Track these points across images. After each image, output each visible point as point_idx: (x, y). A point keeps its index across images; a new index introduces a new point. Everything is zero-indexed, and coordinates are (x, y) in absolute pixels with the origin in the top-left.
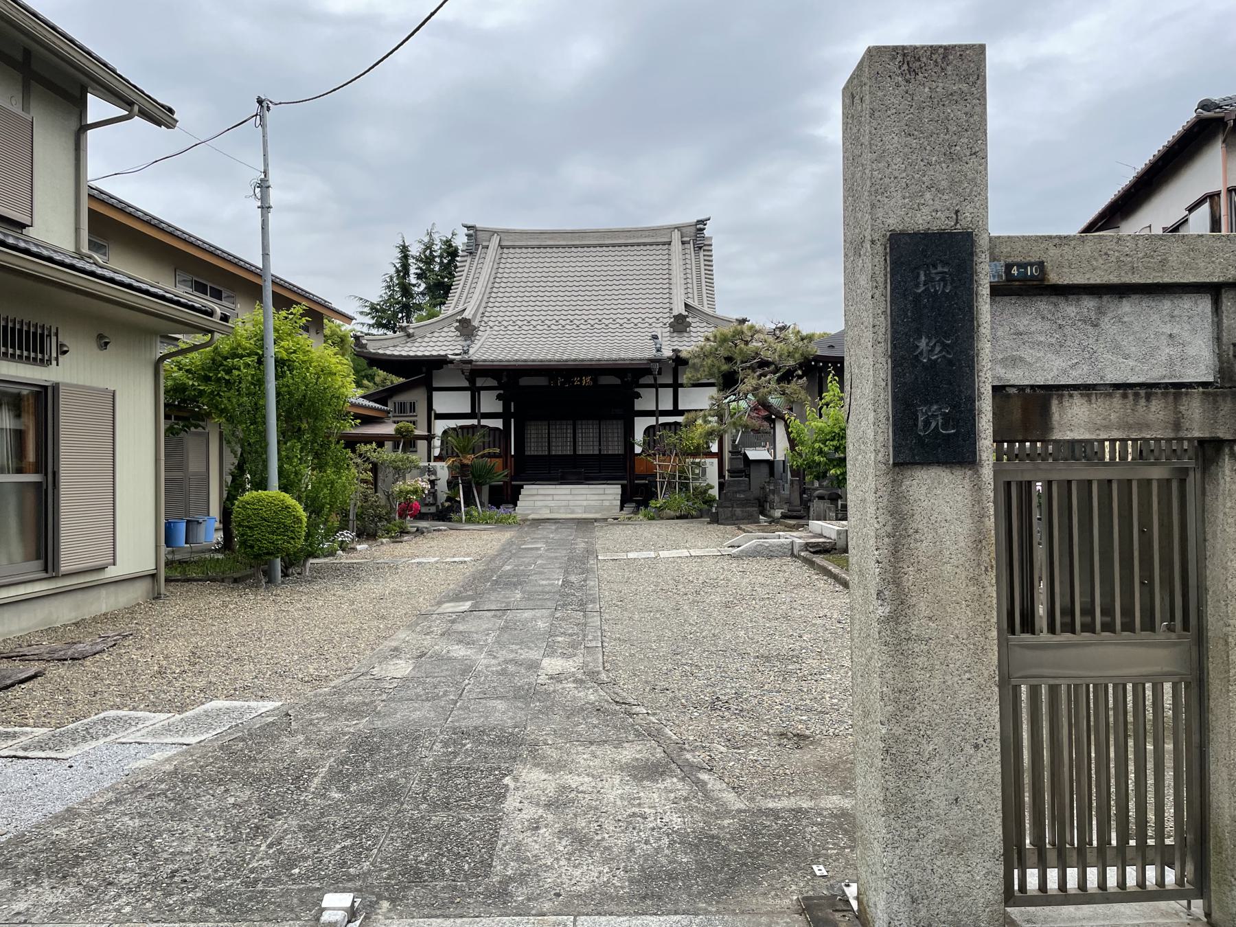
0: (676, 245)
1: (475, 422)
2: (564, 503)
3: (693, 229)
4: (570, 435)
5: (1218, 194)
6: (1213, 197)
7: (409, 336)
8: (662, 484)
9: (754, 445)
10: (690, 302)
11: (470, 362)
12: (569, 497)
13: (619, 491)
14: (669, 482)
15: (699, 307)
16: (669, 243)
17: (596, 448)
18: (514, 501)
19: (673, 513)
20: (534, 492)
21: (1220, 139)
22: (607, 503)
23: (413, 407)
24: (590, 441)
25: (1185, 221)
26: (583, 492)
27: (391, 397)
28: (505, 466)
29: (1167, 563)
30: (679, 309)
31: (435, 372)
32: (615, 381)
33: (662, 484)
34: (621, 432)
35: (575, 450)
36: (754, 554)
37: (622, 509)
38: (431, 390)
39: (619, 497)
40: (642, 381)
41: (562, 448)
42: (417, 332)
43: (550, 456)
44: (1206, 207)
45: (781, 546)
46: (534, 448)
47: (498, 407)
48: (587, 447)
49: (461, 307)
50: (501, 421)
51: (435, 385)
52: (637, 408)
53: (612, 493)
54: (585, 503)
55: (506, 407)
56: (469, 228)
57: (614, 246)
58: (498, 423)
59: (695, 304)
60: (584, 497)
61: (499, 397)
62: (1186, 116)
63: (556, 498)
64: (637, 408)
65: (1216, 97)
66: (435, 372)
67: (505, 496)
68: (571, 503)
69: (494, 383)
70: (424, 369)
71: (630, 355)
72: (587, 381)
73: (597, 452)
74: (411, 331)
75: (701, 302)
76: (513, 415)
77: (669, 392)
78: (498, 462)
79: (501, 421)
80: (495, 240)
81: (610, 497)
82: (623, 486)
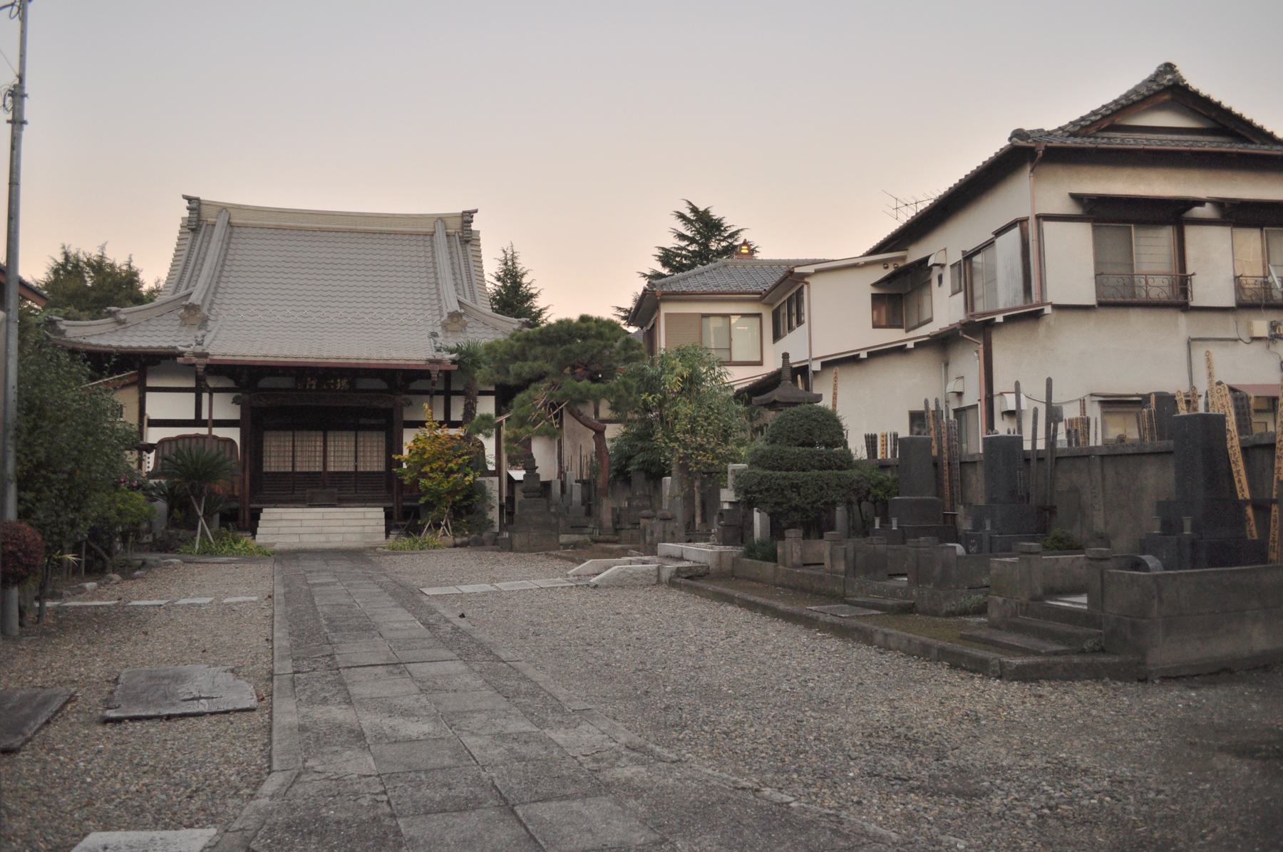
0: (441, 239)
1: (203, 431)
3: (459, 220)
5: (1026, 220)
6: (1020, 223)
7: (121, 322)
9: (156, 458)
10: (462, 299)
11: (206, 355)
12: (321, 523)
13: (382, 515)
15: (474, 305)
16: (432, 235)
18: (252, 525)
20: (277, 516)
21: (1029, 168)
24: (345, 453)
25: (990, 244)
30: (455, 307)
32: (379, 384)
34: (383, 445)
35: (293, 466)
36: (620, 584)
37: (387, 537)
38: (143, 390)
39: (383, 522)
40: (413, 386)
42: (129, 318)
43: (294, 473)
44: (1015, 233)
45: (646, 572)
47: (234, 413)
49: (182, 292)
51: (150, 384)
53: (373, 517)
56: (190, 199)
58: (234, 434)
59: (468, 301)
61: (235, 401)
62: (997, 143)
63: (305, 523)
65: (1028, 127)
67: (241, 519)
69: (231, 384)
70: (137, 365)
71: (405, 356)
72: (342, 384)
73: (352, 469)
74: (122, 317)
75: (474, 299)
77: (440, 400)
81: (373, 523)
82: (385, 509)
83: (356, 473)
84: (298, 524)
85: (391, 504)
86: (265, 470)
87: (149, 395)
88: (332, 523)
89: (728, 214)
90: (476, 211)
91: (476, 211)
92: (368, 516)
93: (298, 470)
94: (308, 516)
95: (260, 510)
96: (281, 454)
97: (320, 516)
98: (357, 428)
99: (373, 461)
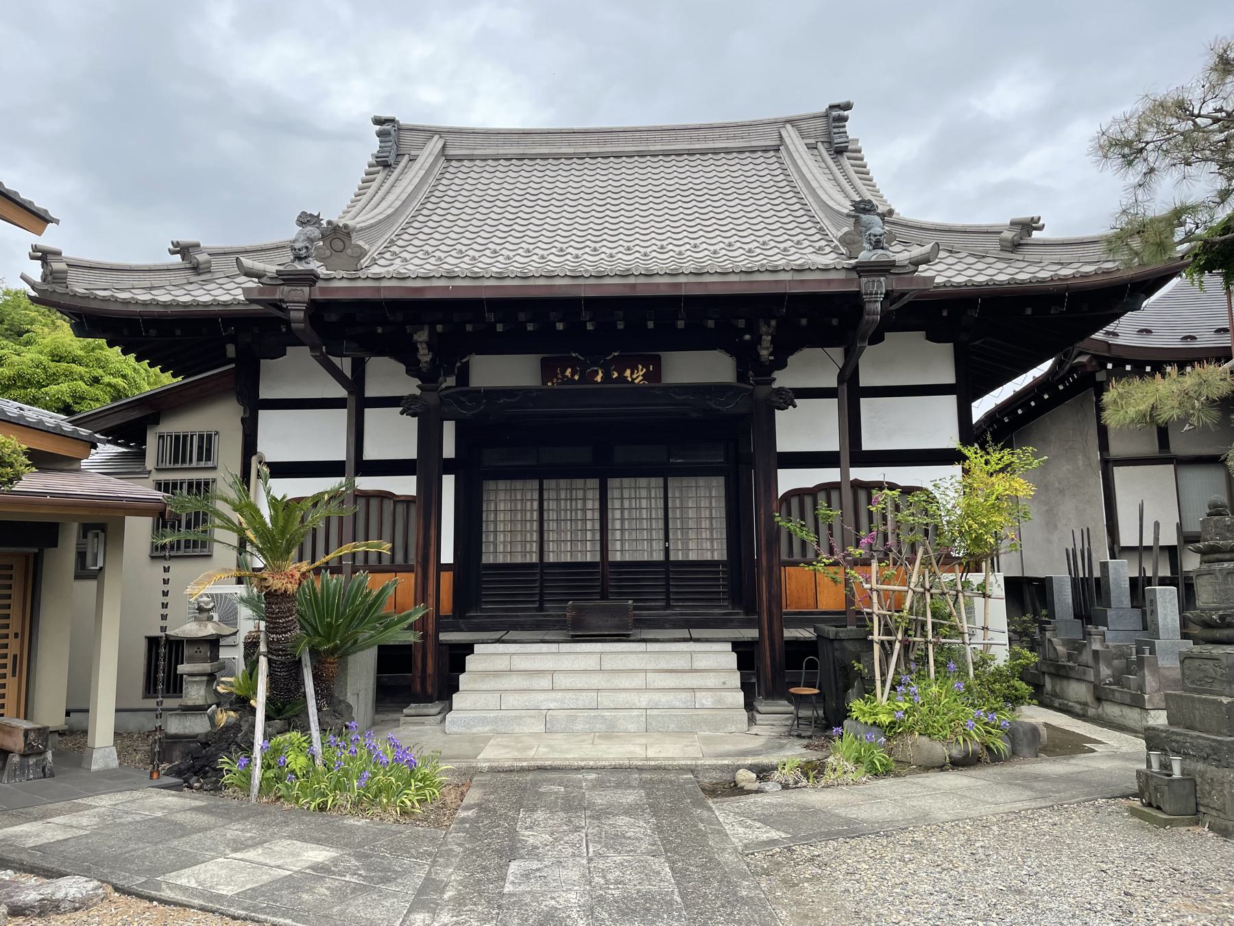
2: (585, 699)
3: (821, 123)
4: (593, 515)
8: (887, 649)
12: (597, 681)
14: (906, 647)
17: (658, 546)
19: (940, 750)
20: (502, 664)
22: (706, 700)
23: (206, 446)
26: (634, 662)
27: (155, 420)
28: (422, 595)
29: (621, 573)
31: (264, 363)
33: (887, 649)
35: (667, 550)
37: (752, 721)
38: (253, 406)
39: (735, 679)
41: (572, 544)
43: (542, 565)
46: (506, 543)
48: (635, 542)
50: (413, 480)
51: (264, 394)
52: (785, 444)
54: (644, 700)
55: (429, 438)
56: (378, 121)
57: (667, 154)
60: (638, 681)
63: (563, 681)
64: (785, 444)
66: (264, 363)
67: (420, 677)
68: (605, 700)
73: (658, 556)
76: (449, 466)
78: (406, 582)
79: (413, 480)
80: (435, 145)
81: (711, 681)
82: (737, 646)
83: (667, 563)
84: (545, 683)
85: (751, 634)
86: (487, 559)
87: (264, 416)
88: (624, 681)
89: (186, 238)
90: (57, 222)
91: (57, 222)
92: (701, 663)
93: (551, 558)
94: (566, 663)
95: (468, 648)
96: (519, 527)
97: (592, 662)
98: (542, 473)
99: (701, 535)
